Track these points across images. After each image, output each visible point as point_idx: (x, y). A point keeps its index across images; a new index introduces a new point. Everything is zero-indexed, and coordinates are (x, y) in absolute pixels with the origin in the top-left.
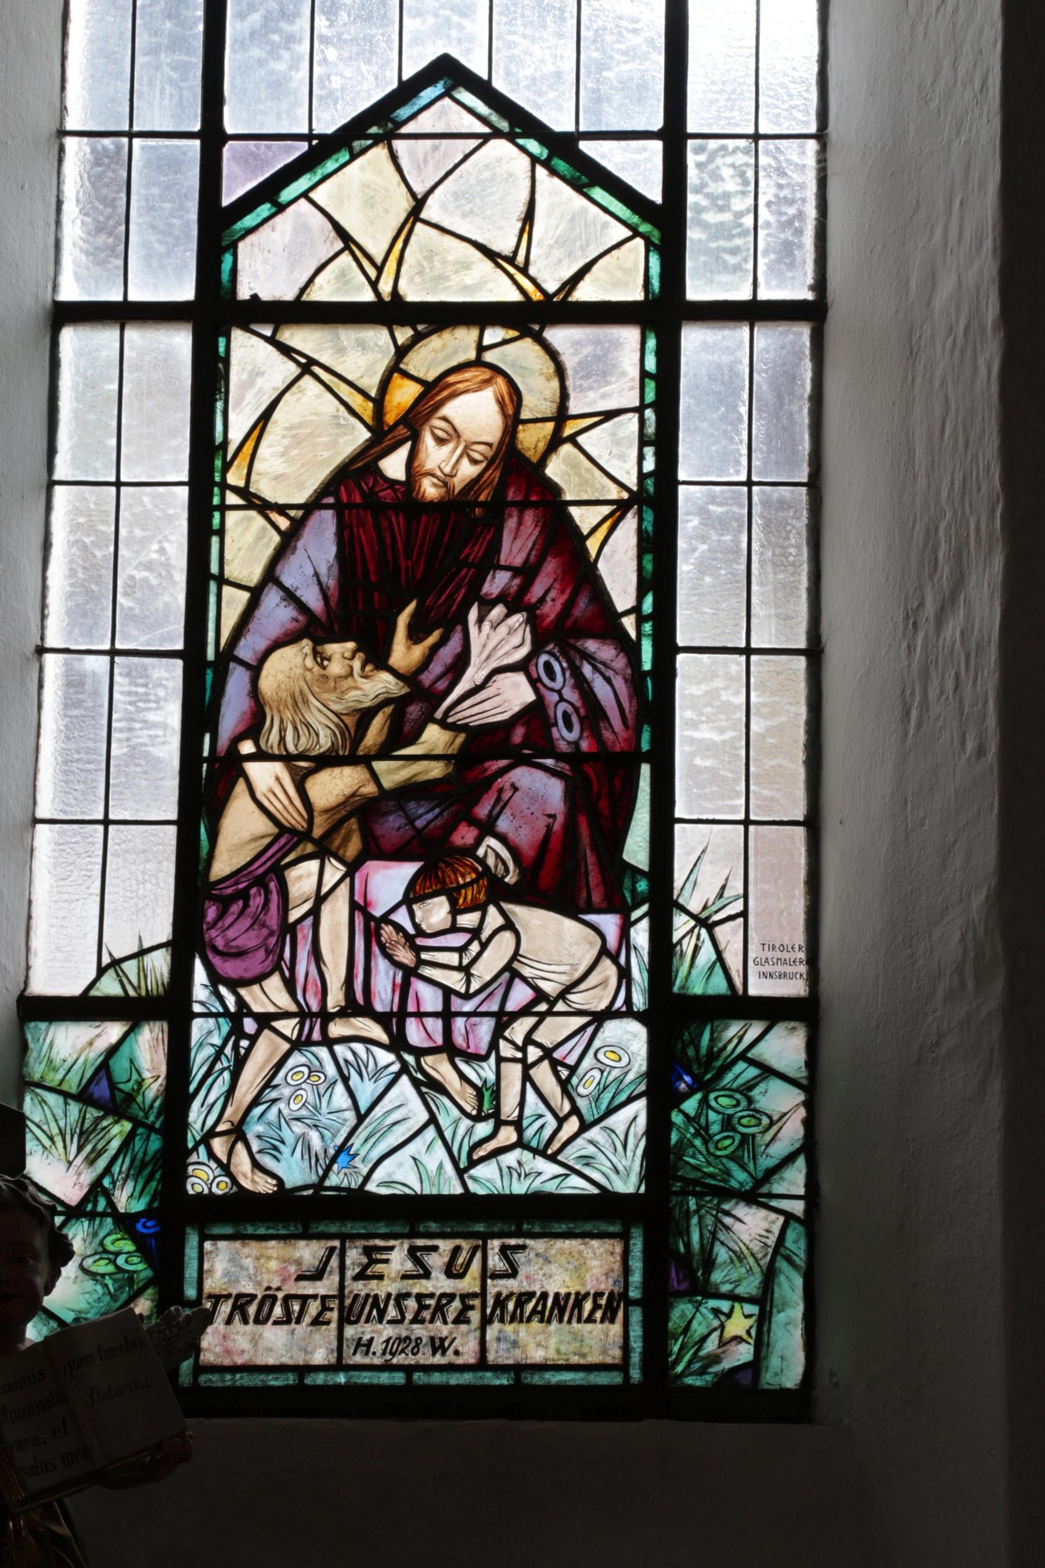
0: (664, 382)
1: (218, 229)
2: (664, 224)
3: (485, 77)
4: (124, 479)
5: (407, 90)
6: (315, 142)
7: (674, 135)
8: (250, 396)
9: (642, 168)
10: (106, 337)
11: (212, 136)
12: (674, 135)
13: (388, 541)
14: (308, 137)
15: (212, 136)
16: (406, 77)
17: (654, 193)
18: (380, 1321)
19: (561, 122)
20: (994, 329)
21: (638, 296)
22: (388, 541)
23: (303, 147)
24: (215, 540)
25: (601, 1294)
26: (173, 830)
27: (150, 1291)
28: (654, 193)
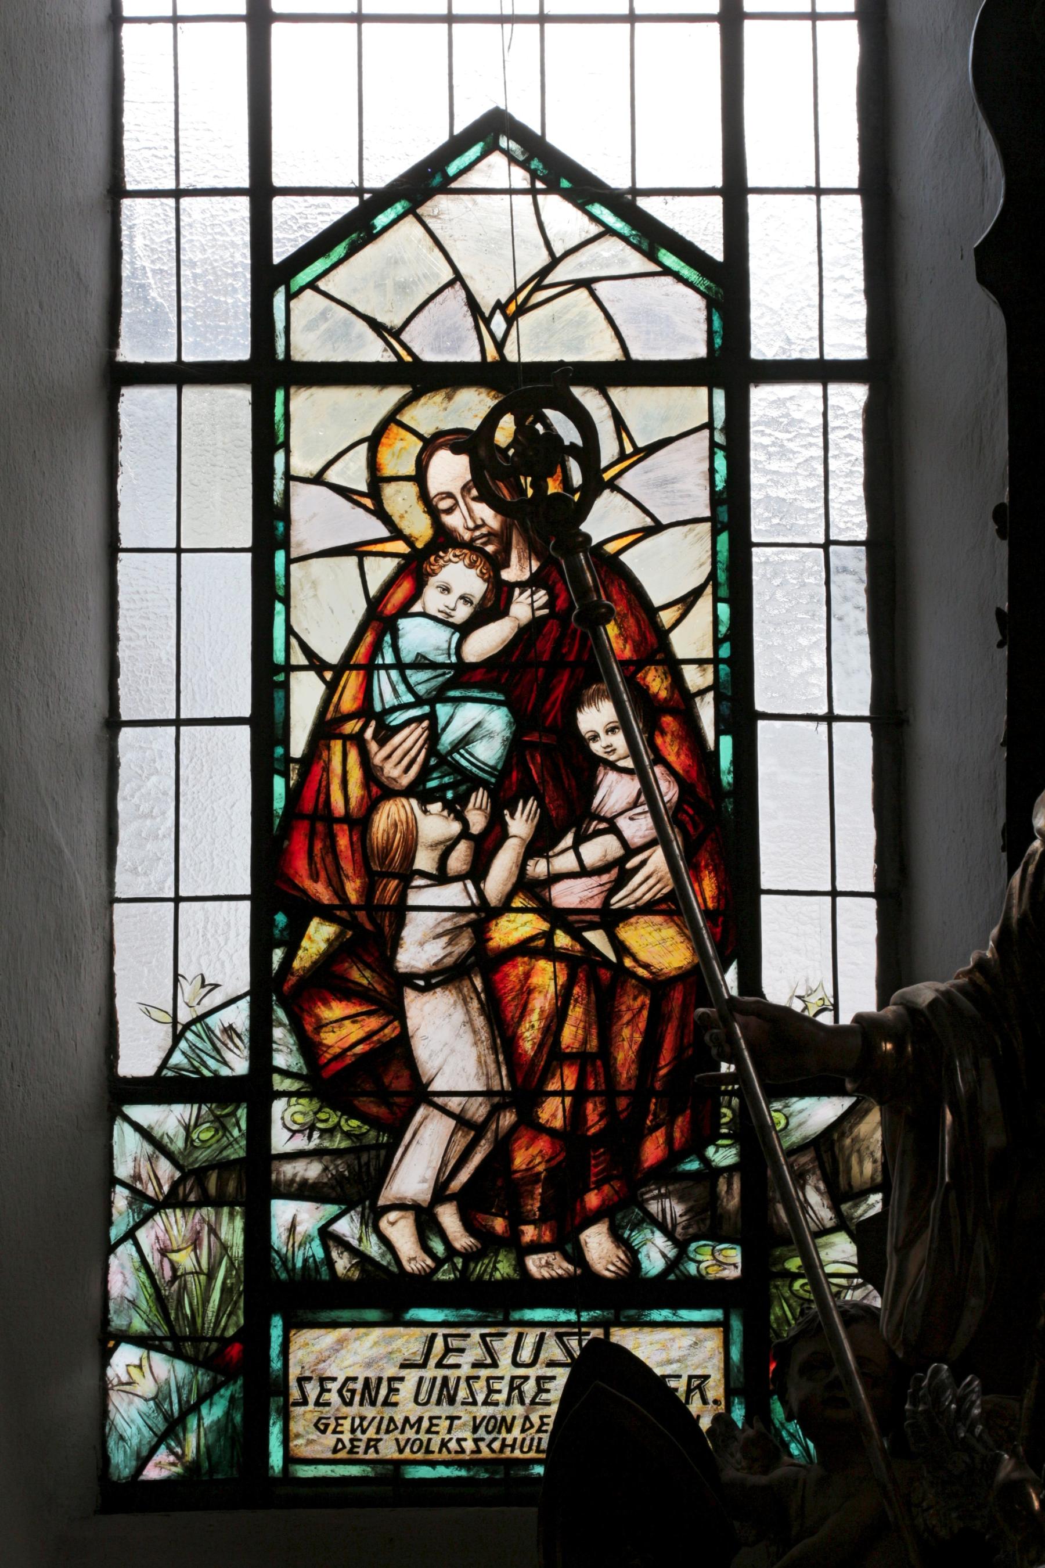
0: (734, 440)
1: (270, 277)
2: (725, 285)
3: (539, 132)
4: (184, 545)
5: (457, 145)
6: (367, 196)
7: (734, 192)
8: (334, 209)
9: (702, 225)
10: (163, 396)
11: (261, 191)
12: (734, 192)
13: (223, 1323)
14: (358, 191)
15: (261, 191)
16: (457, 131)
17: (715, 250)
18: (367, 1380)
19: (617, 179)
20: (533, 1010)
21: (702, 352)
22: (223, 1323)
23: (353, 202)
24: (279, 607)
25: (354, 1379)
26: (246, 906)
27: (578, 947)
28: (715, 250)
